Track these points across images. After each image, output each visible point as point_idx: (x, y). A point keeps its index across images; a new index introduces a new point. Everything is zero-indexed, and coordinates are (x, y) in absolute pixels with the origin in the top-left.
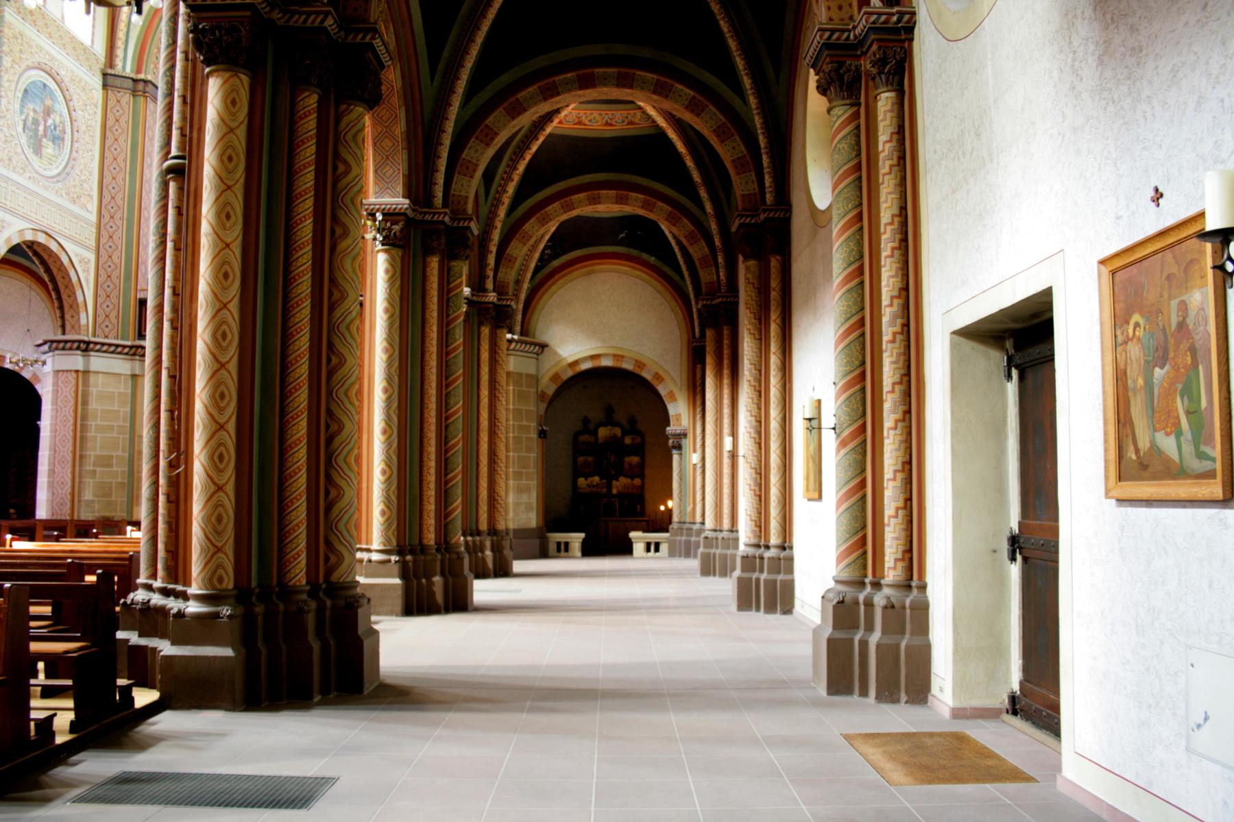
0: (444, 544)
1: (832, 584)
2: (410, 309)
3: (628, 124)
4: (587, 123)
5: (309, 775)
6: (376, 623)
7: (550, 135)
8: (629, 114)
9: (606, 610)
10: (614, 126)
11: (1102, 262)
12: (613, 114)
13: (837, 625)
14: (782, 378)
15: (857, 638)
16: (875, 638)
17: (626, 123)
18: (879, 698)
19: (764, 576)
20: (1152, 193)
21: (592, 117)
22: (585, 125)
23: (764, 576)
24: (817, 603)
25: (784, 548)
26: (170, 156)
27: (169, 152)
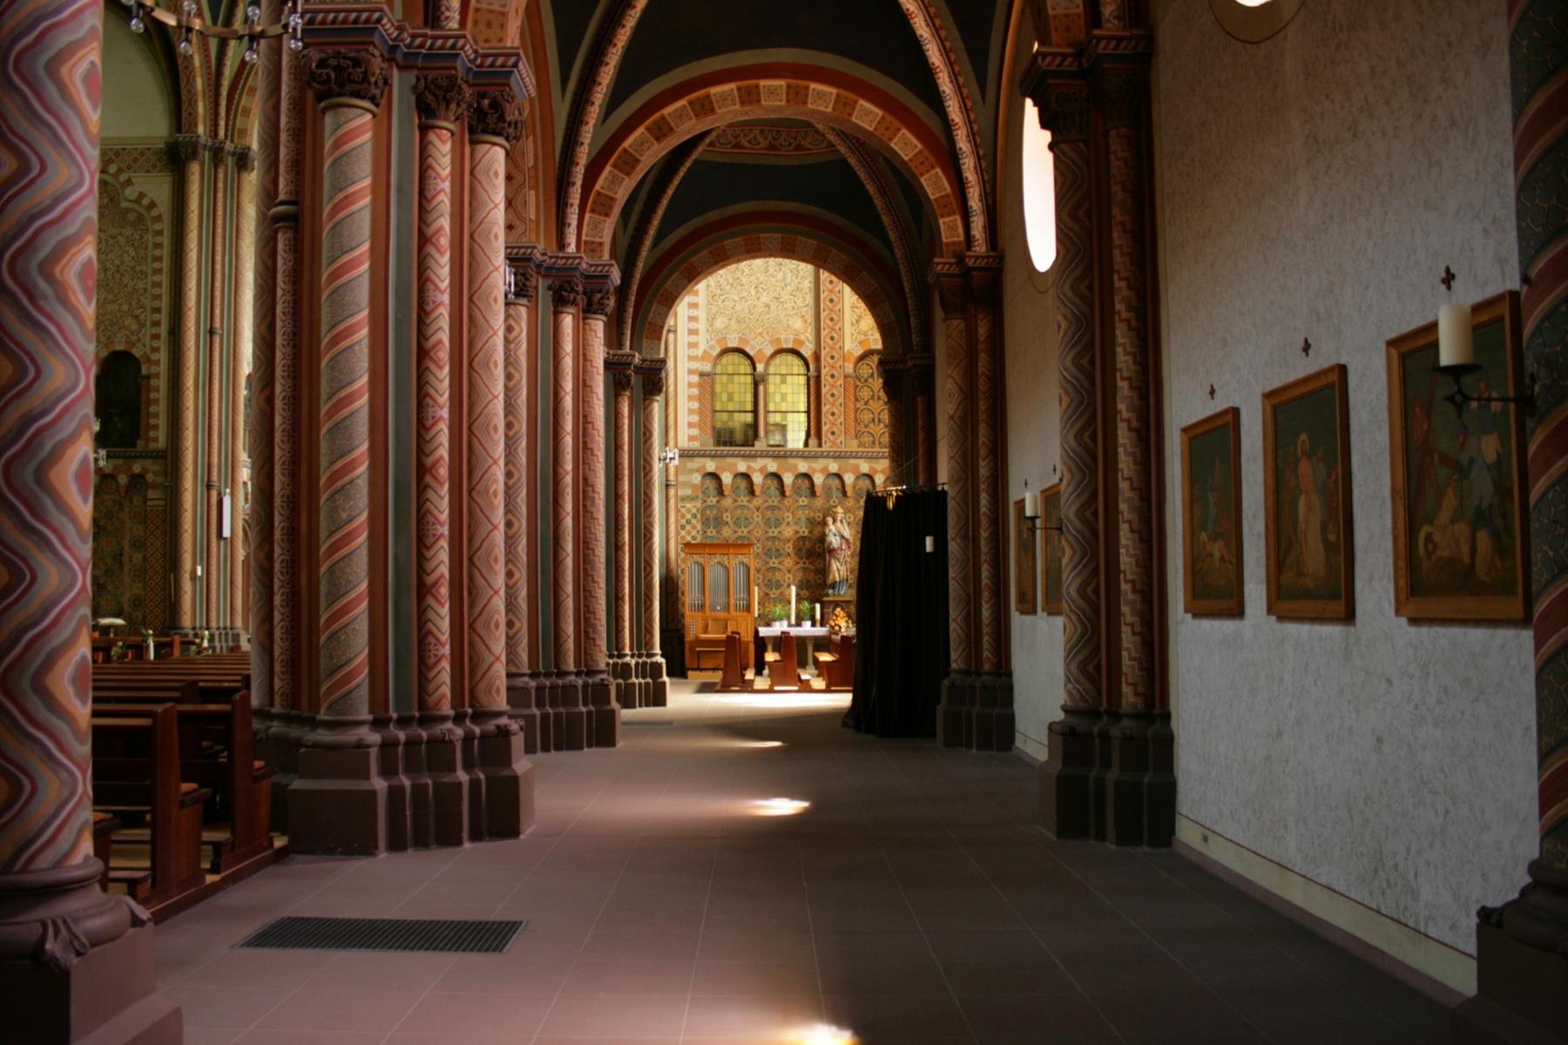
0: (586, 667)
1: (1060, 716)
2: (568, 385)
3: (795, 149)
4: (747, 144)
5: (491, 918)
6: (59, 864)
7: (696, 162)
8: (798, 132)
9: (1410, 545)
10: (778, 149)
11: (1391, 343)
12: (778, 132)
13: (1067, 758)
14: (559, 403)
15: (1093, 774)
16: (1113, 775)
17: (792, 147)
18: (1121, 841)
19: (977, 709)
20: (1443, 275)
21: (752, 136)
22: (744, 148)
23: (977, 709)
24: (1044, 736)
25: (998, 675)
26: (277, 201)
27: (276, 194)
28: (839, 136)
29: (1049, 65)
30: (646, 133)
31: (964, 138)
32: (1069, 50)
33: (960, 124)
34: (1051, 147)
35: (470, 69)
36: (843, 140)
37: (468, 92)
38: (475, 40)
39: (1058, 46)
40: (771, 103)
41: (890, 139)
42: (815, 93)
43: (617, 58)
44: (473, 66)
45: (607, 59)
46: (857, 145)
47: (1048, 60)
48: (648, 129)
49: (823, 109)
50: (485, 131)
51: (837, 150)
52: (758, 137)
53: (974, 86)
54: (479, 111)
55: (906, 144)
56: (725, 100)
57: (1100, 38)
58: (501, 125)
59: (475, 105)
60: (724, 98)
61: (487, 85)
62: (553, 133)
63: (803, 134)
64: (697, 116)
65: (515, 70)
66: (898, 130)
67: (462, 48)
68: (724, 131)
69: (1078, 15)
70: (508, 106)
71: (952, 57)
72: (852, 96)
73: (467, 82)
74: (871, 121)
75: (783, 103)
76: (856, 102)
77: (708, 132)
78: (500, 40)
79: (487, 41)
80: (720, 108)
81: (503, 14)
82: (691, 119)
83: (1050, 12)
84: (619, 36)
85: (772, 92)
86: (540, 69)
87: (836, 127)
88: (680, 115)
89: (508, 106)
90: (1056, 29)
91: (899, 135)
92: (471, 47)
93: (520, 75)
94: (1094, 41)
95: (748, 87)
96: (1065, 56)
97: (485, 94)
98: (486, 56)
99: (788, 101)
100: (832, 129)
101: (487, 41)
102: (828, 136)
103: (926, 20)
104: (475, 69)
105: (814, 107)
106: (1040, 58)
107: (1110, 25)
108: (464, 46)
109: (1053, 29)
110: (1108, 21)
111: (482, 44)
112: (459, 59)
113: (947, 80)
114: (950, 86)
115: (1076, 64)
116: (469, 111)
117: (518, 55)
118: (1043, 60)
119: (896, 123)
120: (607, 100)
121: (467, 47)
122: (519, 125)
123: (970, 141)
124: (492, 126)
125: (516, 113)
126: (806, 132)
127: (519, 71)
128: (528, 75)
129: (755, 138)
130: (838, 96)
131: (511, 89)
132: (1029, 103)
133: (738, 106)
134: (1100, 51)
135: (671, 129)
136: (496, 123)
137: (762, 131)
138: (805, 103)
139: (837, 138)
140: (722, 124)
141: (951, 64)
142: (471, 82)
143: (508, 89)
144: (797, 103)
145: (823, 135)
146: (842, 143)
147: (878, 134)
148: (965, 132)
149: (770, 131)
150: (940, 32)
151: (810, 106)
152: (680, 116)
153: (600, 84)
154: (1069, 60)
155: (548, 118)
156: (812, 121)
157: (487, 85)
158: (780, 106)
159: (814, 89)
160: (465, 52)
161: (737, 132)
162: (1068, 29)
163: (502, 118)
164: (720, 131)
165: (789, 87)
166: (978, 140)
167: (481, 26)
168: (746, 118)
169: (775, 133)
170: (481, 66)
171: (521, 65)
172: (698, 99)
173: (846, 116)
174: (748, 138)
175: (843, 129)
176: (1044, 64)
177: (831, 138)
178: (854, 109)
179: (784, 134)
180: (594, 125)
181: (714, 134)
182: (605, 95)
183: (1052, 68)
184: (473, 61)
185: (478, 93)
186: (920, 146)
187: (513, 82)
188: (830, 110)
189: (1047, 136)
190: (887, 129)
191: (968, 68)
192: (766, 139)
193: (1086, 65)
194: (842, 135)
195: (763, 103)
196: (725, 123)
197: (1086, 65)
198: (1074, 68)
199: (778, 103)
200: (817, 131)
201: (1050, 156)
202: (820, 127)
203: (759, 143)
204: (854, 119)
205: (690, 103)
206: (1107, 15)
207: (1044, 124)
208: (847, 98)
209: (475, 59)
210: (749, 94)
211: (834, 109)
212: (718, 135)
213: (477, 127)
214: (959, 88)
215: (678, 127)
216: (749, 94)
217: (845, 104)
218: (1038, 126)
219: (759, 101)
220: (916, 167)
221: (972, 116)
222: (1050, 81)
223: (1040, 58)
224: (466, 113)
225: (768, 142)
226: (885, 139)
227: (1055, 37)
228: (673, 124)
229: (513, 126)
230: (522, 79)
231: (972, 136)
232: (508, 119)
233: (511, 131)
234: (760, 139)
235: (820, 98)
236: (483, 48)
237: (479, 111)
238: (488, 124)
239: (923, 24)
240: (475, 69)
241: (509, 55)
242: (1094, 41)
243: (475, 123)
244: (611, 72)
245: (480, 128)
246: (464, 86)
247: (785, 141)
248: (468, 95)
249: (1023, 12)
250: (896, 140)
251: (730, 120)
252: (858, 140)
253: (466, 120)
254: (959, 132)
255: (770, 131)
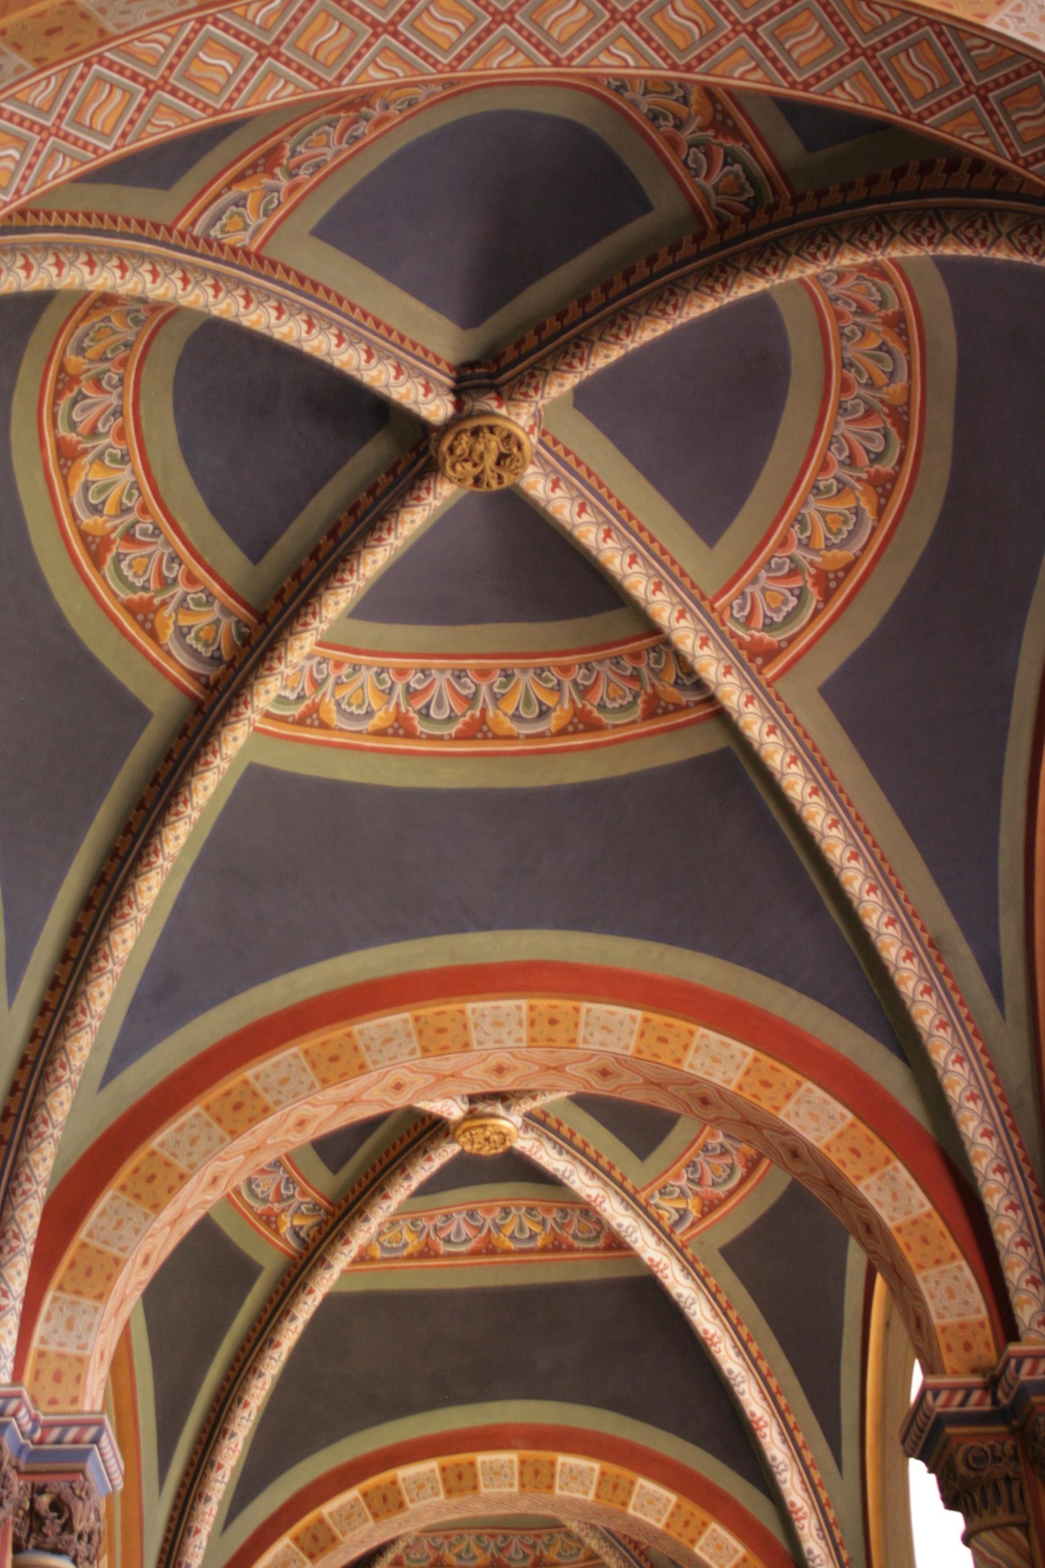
12: (505, 1537)
21: (463, 1546)
28: (606, 1540)
29: (947, 1404)
30: (293, 1546)
31: (814, 1532)
32: (976, 1379)
33: (806, 1509)
34: (967, 1539)
35: (22, 1448)
36: (611, 1545)
37: (17, 1483)
38: (34, 1401)
39: (955, 1373)
40: (496, 1490)
41: (693, 1541)
42: (567, 1471)
43: (249, 1424)
44: (29, 1442)
45: (233, 1427)
46: (636, 1553)
47: (943, 1397)
48: (296, 1540)
49: (579, 1496)
50: (38, 1548)
51: (604, 1564)
52: (473, 1546)
53: (822, 1446)
54: (33, 1513)
55: (719, 1547)
56: (421, 1487)
57: (1020, 1360)
58: (66, 1536)
59: (27, 1505)
60: (419, 1484)
61: (48, 1472)
62: (142, 1547)
63: (546, 1538)
64: (376, 1515)
65: (95, 1447)
66: (705, 1524)
67: (14, 1415)
68: (417, 1539)
69: (982, 1325)
70: (80, 1505)
71: (782, 1401)
72: (626, 1474)
73: (16, 1468)
74: (660, 1512)
75: (516, 1489)
76: (632, 1483)
77: (393, 1542)
78: (74, 1401)
79: (53, 1402)
80: (412, 1501)
81: (80, 1360)
82: (366, 1520)
83: (936, 1321)
84: (253, 1391)
85: (496, 1472)
86: (127, 1443)
87: (599, 1524)
88: (347, 1516)
89: (80, 1505)
90: (949, 1349)
91: (707, 1533)
92: (28, 1411)
93: (102, 1455)
94: (1013, 1363)
95: (458, 1465)
96: (969, 1390)
97: (45, 1486)
98: (48, 1426)
99: (522, 1485)
100: (593, 1527)
101: (53, 1402)
102: (587, 1540)
103: (735, 1346)
104: (32, 1447)
105: (566, 1493)
106: (929, 1396)
107: (1033, 1336)
108: (18, 1409)
109: (943, 1348)
110: (1030, 1329)
111: (44, 1407)
112: (7, 1435)
113: (777, 1439)
114: (784, 1448)
115: (988, 1400)
116: (17, 1515)
117: (100, 1424)
118: (935, 1397)
119: (701, 1514)
120: (231, 1494)
121: (23, 1413)
122: (95, 1538)
123: (824, 1538)
124: (52, 1539)
125: (92, 1517)
126: (551, 1536)
127: (100, 1449)
128: (115, 1455)
129: (468, 1550)
130: (603, 1474)
131: (85, 1478)
132: (917, 1470)
133: (442, 1496)
134: (1024, 1376)
135: (334, 1539)
136: (59, 1535)
137: (479, 1537)
138: (550, 1487)
139: (602, 1543)
140: (412, 1528)
141: (781, 1414)
142: (23, 1467)
143: (81, 1478)
144: (536, 1487)
145: (579, 1540)
146: (611, 1552)
147: (673, 1533)
148: (814, 1523)
149: (492, 1536)
150: (760, 1362)
151: (558, 1491)
152: (349, 1517)
153: (220, 1467)
154: (976, 1396)
155: (134, 1526)
156: (562, 1517)
157: (48, 1472)
158: (510, 1494)
159: (563, 1465)
160: (17, 1420)
161: (439, 1541)
162: (967, 1347)
163: (68, 1526)
164: (410, 1541)
165: (523, 1462)
166: (838, 1535)
167: (46, 1378)
168: (456, 1516)
169: (500, 1539)
170: (41, 1442)
171: (104, 1441)
172: (378, 1487)
173: (619, 1507)
174: (456, 1550)
175: (612, 1528)
176: (938, 1405)
177: (593, 1543)
178: (630, 1494)
179: (515, 1541)
180: (209, 1536)
181: (401, 1545)
182: (228, 1485)
183: (953, 1408)
184: (29, 1435)
185: (33, 1485)
186: (742, 1551)
187: (90, 1467)
188: (591, 1497)
189: (956, 1521)
190: (687, 1524)
191: (801, 1402)
192: (485, 1549)
193: (1005, 1401)
194: (610, 1537)
195: (483, 1490)
196: (421, 1525)
197: (1005, 1401)
198: (987, 1407)
199: (506, 1490)
200: (569, 1534)
201: (967, 1552)
202: (574, 1526)
203: (474, 1557)
204: (631, 1511)
205: (365, 1495)
206: (1026, 1320)
207: (951, 1501)
208: (617, 1476)
209: (34, 1431)
210: (460, 1477)
211: (598, 1496)
212: (408, 1547)
213: (27, 1540)
214: (798, 1452)
215: (344, 1533)
216: (460, 1477)
217: (615, 1487)
218: (940, 1504)
219: (475, 1488)
220: (680, 1535)
221: (824, 1495)
222: (949, 1430)
223: (929, 1396)
224: (11, 1517)
225: (488, 1555)
226: (685, 1541)
227: (949, 1361)
228: (337, 1531)
229: (85, 1538)
230: (104, 1461)
231: (828, 1527)
232: (79, 1527)
233: (82, 1547)
234: (475, 1550)
235: (574, 1479)
236: (45, 1414)
237: (33, 1513)
238: (46, 1536)
239: (732, 1352)
240: (32, 1447)
241: (85, 1425)
242: (1013, 1363)
243: (24, 1535)
244: (240, 1447)
245: (32, 1541)
246: (12, 1475)
247: (517, 1551)
248: (16, 1489)
249: (887, 1325)
250: (701, 1542)
251: (429, 1520)
252: (637, 1545)
253: (11, 1530)
254: (805, 1522)
255: (492, 1536)
